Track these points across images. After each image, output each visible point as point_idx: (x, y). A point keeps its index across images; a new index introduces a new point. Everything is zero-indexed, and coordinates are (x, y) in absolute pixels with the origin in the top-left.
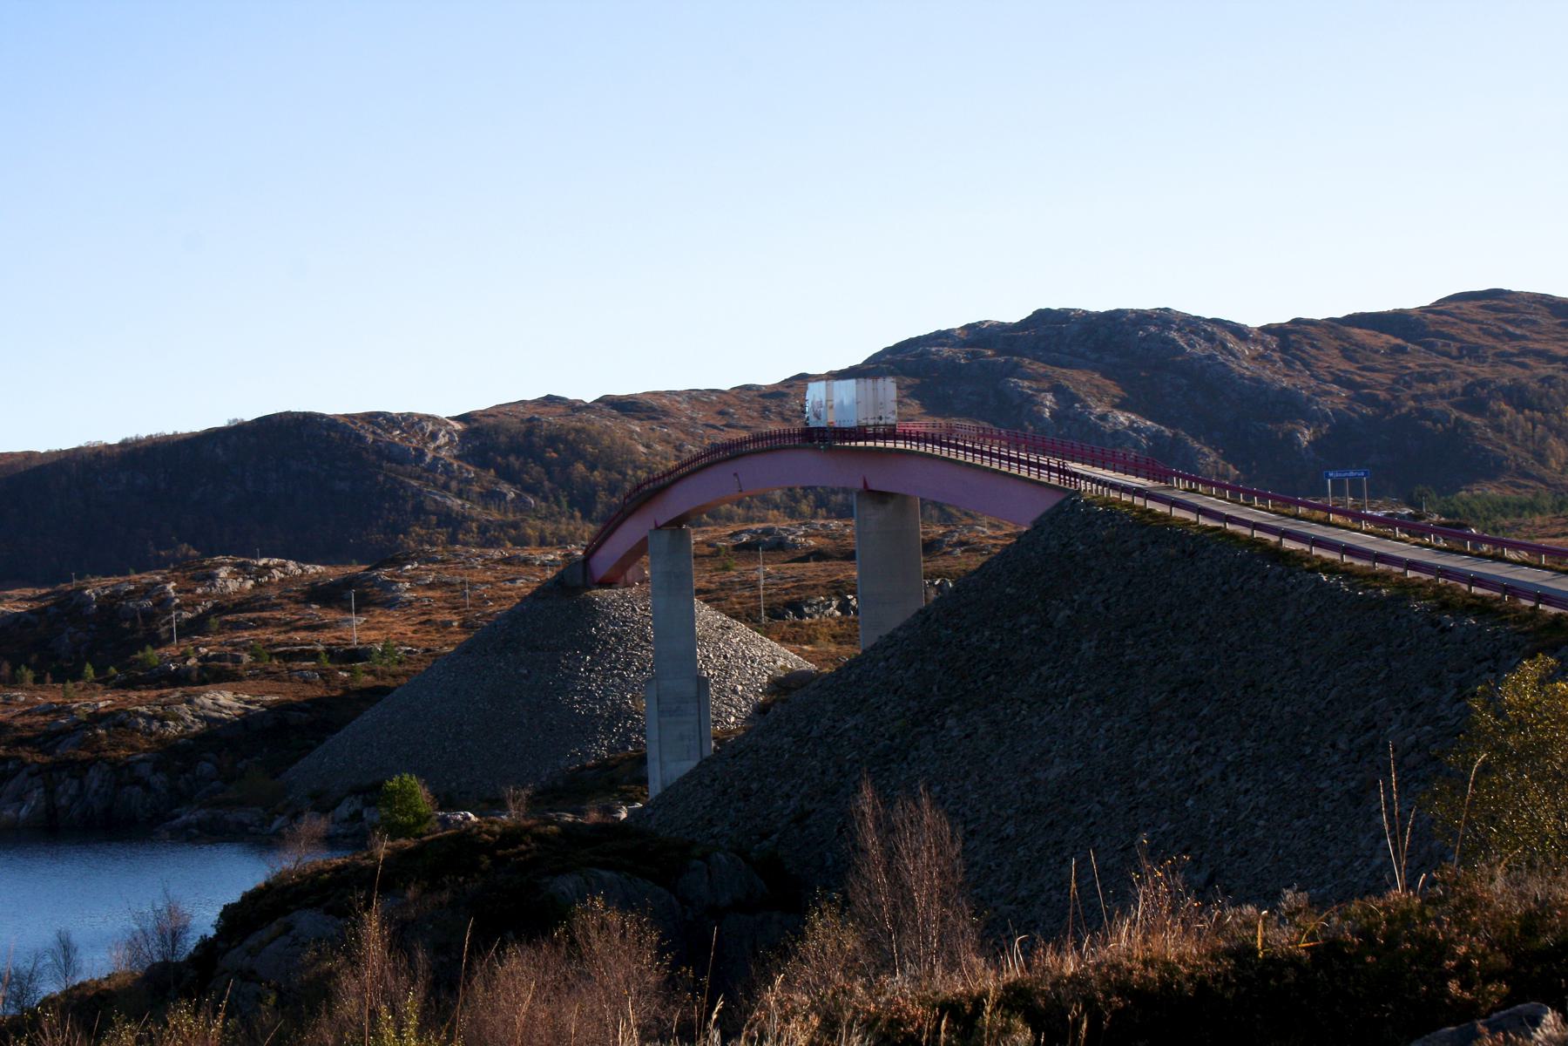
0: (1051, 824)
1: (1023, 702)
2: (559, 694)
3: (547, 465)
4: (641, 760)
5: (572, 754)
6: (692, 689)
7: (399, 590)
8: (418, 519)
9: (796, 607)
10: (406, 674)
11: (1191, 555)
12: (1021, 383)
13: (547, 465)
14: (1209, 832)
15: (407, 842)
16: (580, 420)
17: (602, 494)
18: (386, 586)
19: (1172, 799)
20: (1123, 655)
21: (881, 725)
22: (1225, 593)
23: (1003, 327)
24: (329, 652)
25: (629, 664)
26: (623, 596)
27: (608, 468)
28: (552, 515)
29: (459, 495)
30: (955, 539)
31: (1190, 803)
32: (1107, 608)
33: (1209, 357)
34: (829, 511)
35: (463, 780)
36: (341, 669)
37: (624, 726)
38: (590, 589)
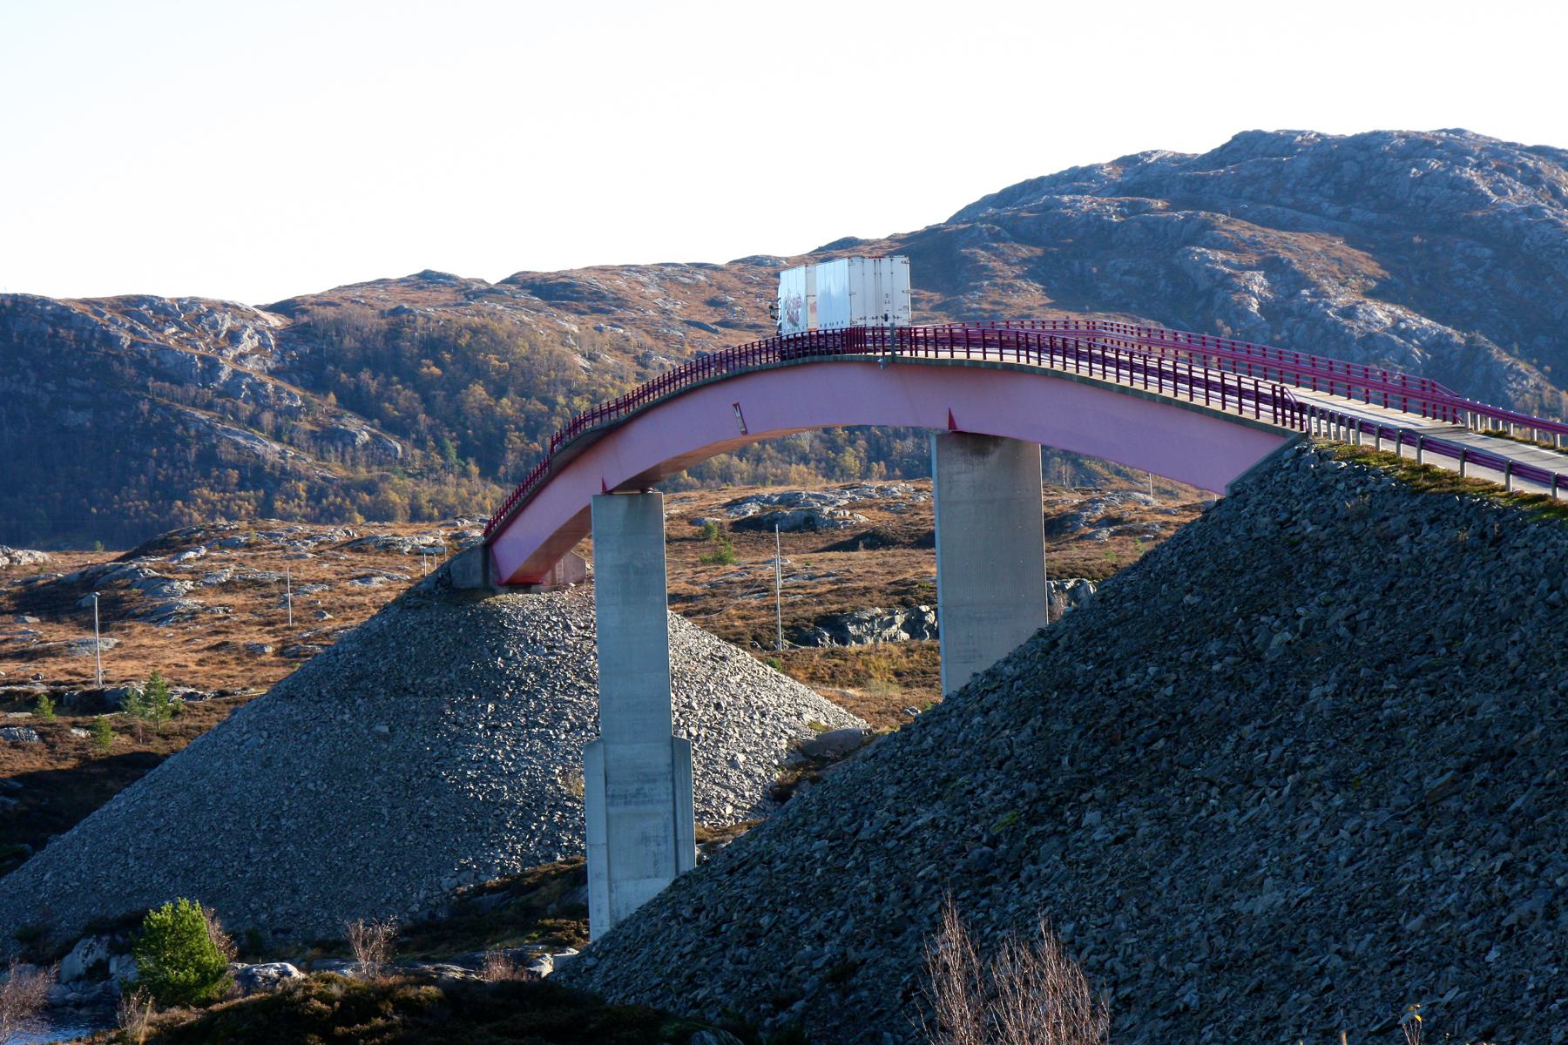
0: (1258, 989)
1: (1212, 784)
2: (441, 767)
3: (424, 389)
4: (578, 877)
5: (463, 868)
6: (662, 759)
7: (174, 593)
8: (206, 475)
9: (835, 625)
10: (185, 733)
11: (1497, 541)
12: (1210, 254)
13: (424, 389)
14: (1525, 1005)
15: (184, 1014)
16: (479, 313)
17: (514, 436)
18: (152, 586)
19: (1463, 948)
20: (1379, 707)
21: (976, 820)
22: (1553, 606)
23: (1182, 162)
24: (55, 695)
25: (558, 717)
26: (549, 606)
27: (525, 394)
28: (431, 470)
29: (277, 436)
30: (1099, 514)
31: (1493, 955)
32: (1353, 630)
33: (1529, 211)
34: (891, 466)
35: (280, 909)
36: (75, 725)
37: (550, 820)
38: (494, 593)
